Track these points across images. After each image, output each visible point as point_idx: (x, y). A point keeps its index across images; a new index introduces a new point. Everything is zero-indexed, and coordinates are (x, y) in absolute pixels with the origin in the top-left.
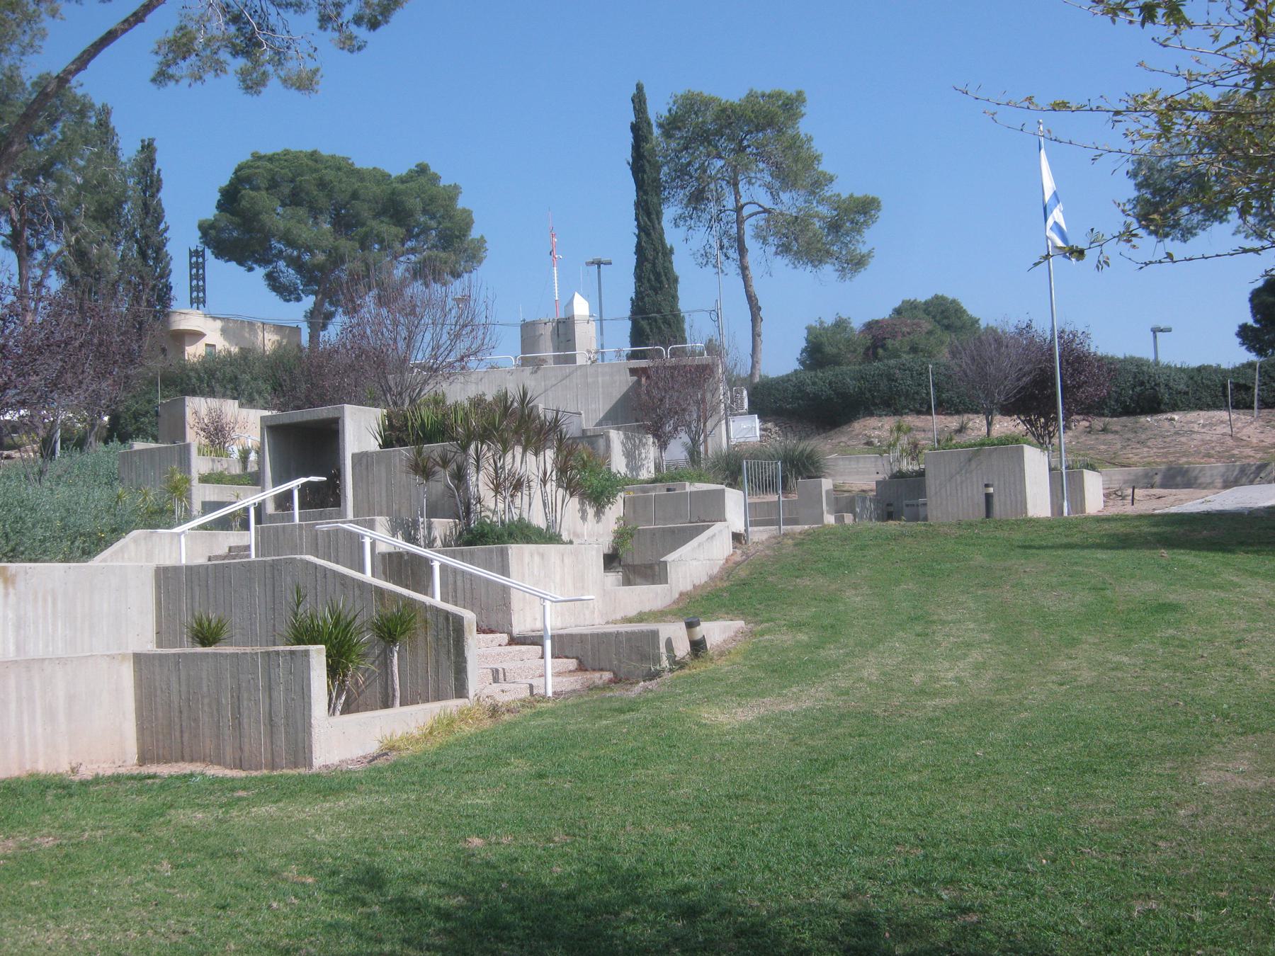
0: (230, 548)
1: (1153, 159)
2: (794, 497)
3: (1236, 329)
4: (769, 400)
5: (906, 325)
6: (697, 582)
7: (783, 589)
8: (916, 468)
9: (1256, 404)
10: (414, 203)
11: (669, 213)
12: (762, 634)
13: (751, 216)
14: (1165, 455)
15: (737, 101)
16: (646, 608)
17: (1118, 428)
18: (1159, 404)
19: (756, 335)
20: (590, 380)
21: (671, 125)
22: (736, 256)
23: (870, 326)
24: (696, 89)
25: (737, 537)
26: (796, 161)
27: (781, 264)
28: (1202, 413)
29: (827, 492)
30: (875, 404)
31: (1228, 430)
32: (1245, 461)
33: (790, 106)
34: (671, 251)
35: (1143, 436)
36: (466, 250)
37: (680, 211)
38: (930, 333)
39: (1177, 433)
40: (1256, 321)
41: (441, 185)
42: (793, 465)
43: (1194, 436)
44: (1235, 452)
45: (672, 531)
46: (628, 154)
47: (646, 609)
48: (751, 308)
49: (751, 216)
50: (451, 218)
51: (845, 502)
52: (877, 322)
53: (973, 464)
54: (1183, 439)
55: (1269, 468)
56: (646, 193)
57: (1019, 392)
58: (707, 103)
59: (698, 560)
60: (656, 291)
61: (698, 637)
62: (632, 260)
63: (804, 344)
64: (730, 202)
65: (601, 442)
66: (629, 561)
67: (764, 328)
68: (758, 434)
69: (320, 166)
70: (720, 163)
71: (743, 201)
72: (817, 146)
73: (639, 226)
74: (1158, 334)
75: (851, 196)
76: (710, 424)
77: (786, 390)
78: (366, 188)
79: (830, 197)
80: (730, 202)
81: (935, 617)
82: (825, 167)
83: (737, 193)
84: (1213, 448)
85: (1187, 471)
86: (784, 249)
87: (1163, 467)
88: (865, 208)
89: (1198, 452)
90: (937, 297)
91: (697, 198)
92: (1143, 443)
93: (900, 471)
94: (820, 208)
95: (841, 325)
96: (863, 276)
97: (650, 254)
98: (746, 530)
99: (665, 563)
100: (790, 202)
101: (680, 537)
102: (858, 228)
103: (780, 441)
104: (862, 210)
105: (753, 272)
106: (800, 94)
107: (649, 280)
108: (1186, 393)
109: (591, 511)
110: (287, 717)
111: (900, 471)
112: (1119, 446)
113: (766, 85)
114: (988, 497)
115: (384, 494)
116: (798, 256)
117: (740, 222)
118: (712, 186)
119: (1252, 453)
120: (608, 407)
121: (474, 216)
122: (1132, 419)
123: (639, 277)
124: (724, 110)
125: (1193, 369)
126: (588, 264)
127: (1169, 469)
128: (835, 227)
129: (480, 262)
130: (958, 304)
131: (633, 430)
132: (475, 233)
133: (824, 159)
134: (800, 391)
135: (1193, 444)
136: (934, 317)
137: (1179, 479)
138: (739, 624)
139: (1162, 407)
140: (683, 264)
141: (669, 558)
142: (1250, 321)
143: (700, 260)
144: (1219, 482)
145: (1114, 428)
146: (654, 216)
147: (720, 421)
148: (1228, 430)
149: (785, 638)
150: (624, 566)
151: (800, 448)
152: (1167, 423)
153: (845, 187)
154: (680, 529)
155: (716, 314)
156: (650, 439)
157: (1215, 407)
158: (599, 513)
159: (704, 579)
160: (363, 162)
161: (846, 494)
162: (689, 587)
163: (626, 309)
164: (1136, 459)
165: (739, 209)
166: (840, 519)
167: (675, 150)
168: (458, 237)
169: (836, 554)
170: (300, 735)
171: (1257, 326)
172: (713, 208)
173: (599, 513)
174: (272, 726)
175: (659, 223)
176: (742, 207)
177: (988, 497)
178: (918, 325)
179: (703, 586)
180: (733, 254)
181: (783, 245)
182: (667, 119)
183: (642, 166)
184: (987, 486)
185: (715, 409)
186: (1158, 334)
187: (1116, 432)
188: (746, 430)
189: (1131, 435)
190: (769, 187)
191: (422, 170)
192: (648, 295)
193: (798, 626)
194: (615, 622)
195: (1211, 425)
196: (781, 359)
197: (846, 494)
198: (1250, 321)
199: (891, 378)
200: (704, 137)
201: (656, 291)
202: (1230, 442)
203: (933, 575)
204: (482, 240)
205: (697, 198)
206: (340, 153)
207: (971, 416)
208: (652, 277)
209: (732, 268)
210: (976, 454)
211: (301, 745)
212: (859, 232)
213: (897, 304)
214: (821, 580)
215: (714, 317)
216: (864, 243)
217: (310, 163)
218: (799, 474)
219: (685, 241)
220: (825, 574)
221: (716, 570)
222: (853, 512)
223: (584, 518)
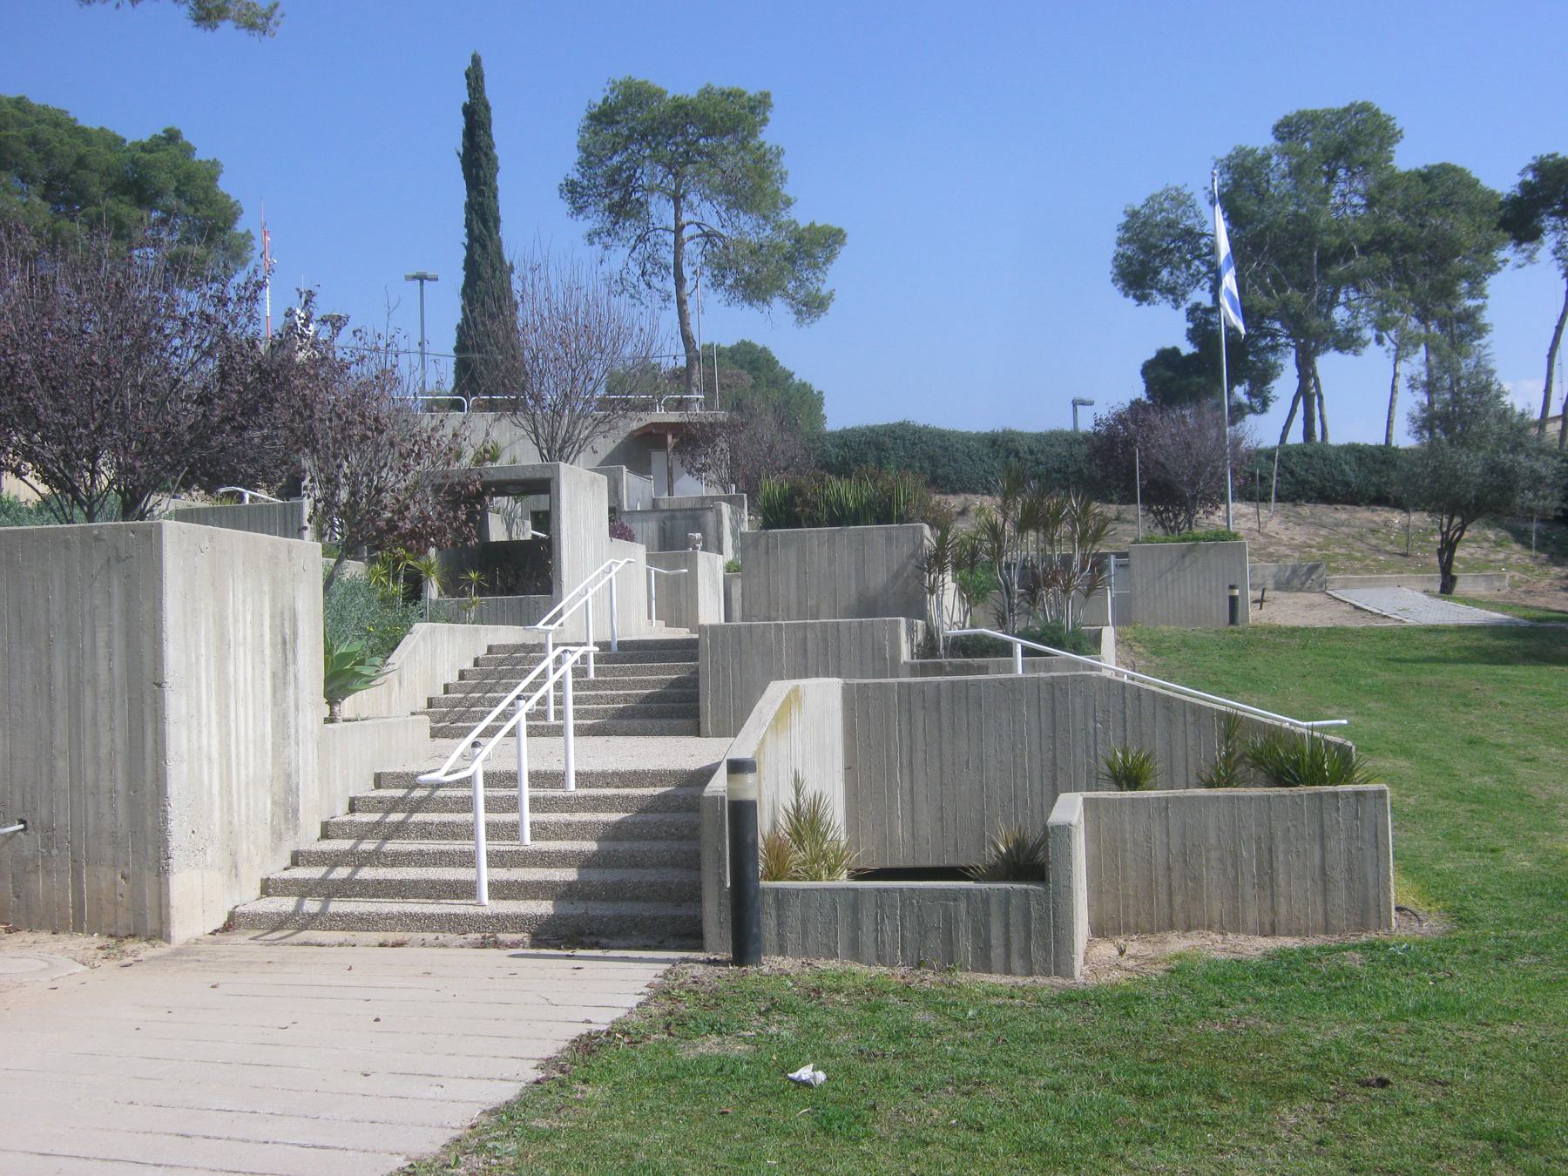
0: (490, 649)
10: (162, 178)
13: (692, 238)
40: (1149, 397)
41: (196, 159)
46: (457, 142)
53: (1187, 562)
62: (460, 278)
69: (31, 119)
73: (470, 235)
78: (98, 153)
90: (743, 343)
96: (824, 321)
100: (747, 228)
104: (819, 244)
110: (1350, 870)
113: (723, 81)
114: (1233, 599)
115: (793, 585)
119: (1288, 552)
130: (769, 353)
132: (240, 227)
153: (804, 213)
160: (89, 119)
163: (451, 340)
170: (1372, 893)
174: (1325, 882)
177: (1233, 599)
183: (477, 159)
184: (1232, 587)
191: (172, 137)
206: (56, 103)
210: (1190, 549)
211: (1372, 902)
217: (17, 113)
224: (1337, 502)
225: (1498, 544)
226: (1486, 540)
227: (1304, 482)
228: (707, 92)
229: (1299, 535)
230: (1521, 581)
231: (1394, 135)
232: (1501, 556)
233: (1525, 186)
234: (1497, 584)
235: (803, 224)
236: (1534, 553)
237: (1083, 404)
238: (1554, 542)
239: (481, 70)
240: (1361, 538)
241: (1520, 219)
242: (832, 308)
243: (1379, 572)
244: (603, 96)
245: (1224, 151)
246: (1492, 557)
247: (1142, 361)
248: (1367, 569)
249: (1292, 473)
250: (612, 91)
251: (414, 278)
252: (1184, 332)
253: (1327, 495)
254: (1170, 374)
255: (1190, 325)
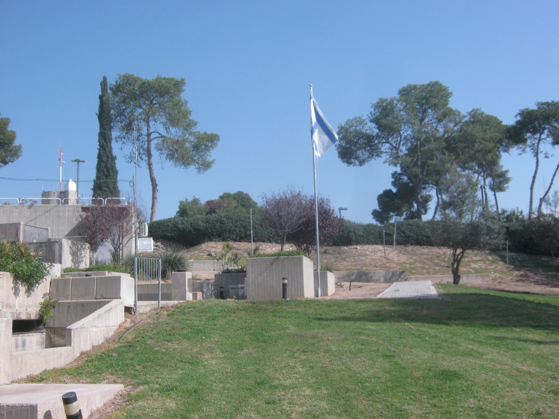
1: (347, 126)
2: (169, 282)
3: (372, 211)
4: (158, 231)
5: (226, 203)
6: (96, 344)
7: (158, 351)
8: (236, 268)
9: (394, 242)
11: (115, 134)
12: (137, 398)
13: (155, 138)
14: (356, 265)
15: (151, 80)
16: (51, 366)
17: (331, 252)
18: (350, 241)
19: (154, 198)
20: (61, 214)
21: (117, 89)
22: (146, 158)
23: (209, 203)
24: (130, 73)
25: (128, 310)
26: (179, 112)
27: (169, 164)
28: (370, 246)
29: (189, 280)
30: (213, 235)
31: (383, 255)
32: (394, 270)
33: (178, 85)
34: (115, 158)
35: (344, 256)
36: (11, 151)
37: (118, 134)
38: (236, 207)
39: (359, 255)
40: (380, 208)
42: (170, 264)
43: (368, 257)
44: (388, 265)
45: (83, 304)
46: (96, 109)
47: (50, 367)
48: (152, 185)
49: (155, 138)
50: (4, 134)
51: (198, 286)
52: (212, 201)
53: (274, 266)
54: (363, 258)
55: (405, 273)
56: (105, 129)
57: (299, 227)
58: (136, 80)
59: (95, 329)
60: (107, 177)
61: (74, 412)
62: (96, 161)
63: (178, 209)
64: (144, 131)
65: (57, 246)
66: (51, 325)
67: (158, 195)
68: (152, 247)
70: (140, 111)
71: (151, 131)
72: (190, 106)
73: (100, 145)
74: (342, 211)
75: (205, 133)
76: (125, 240)
77: (168, 226)
79: (195, 133)
80: (144, 131)
81: (276, 382)
82: (192, 117)
83: (148, 126)
84: (377, 263)
85: (367, 274)
86: (171, 156)
87: (356, 271)
88: (212, 139)
89: (370, 265)
90: (239, 192)
91: (128, 128)
92: (344, 259)
93: (228, 269)
94: (190, 137)
95: (196, 201)
96: (209, 172)
97: (104, 159)
98: (135, 305)
99: (70, 330)
100: (175, 133)
101: (86, 309)
102: (207, 148)
103: (163, 251)
105: (155, 167)
106: (183, 80)
107: (103, 171)
108: (363, 236)
109: (22, 289)
111: (228, 269)
112: (333, 260)
114: (284, 285)
116: (177, 160)
117: (149, 141)
118: (136, 122)
119: (395, 266)
120: (70, 229)
121: (17, 135)
122: (337, 248)
123: (98, 170)
124: (144, 83)
125: (365, 226)
126: (73, 161)
127: (359, 273)
128: (196, 147)
129: (18, 157)
131: (77, 240)
132: (16, 143)
133: (193, 113)
134: (175, 227)
135: (368, 260)
136: (238, 201)
137: (363, 277)
138: (119, 387)
139: (352, 242)
140: (121, 165)
141: (73, 326)
142: (377, 208)
143: (128, 160)
144: (382, 279)
145: (330, 252)
146: (108, 141)
147: (131, 238)
148: (383, 255)
149: (156, 404)
150: (47, 328)
151: (174, 255)
152: (354, 250)
153: (204, 127)
154: (88, 303)
155: (133, 184)
156: (88, 245)
157: (376, 243)
158: (29, 290)
159: (101, 340)
161: (198, 281)
162: (89, 348)
164: (341, 267)
165: (149, 135)
166: (195, 296)
167: (117, 102)
168: (7, 144)
169: (196, 323)
171: (380, 210)
172: (135, 133)
173: (29, 290)
175: (110, 144)
176: (151, 134)
178: (231, 203)
179: (100, 347)
180: (145, 158)
181: (170, 154)
182: (115, 86)
184: (284, 279)
185: (128, 232)
186: (342, 211)
187: (331, 254)
188: (146, 245)
189: (338, 255)
190: (164, 124)
192: (103, 179)
193: (166, 390)
194: (18, 382)
195: (375, 252)
196: (167, 211)
197: (198, 281)
198: (377, 208)
199: (222, 222)
200: (133, 96)
201: (107, 177)
202: (385, 260)
203: (264, 341)
204: (20, 147)
205: (128, 128)
207: (261, 243)
208: (105, 170)
209: (144, 165)
210: (275, 260)
212: (209, 151)
213: (221, 194)
214: (186, 344)
215: (132, 184)
216: (210, 156)
218: (173, 269)
219: (121, 150)
220: (188, 339)
221: (111, 334)
222: (202, 291)
223: (16, 293)
224: (425, 245)
225: (493, 262)
226: (488, 260)
227: (408, 237)
228: (158, 79)
229: (403, 258)
230: (499, 278)
231: (448, 95)
232: (493, 267)
233: (518, 123)
234: (486, 279)
235: (202, 132)
236: (507, 265)
237: (343, 209)
238: (519, 261)
239: (106, 82)
240: (431, 260)
241: (515, 136)
242: (214, 167)
243: (433, 274)
244: (115, 80)
245: (375, 101)
246: (489, 267)
247: (377, 195)
248: (429, 273)
249: (404, 233)
250: (119, 78)
251: (75, 161)
252: (391, 183)
253: (419, 242)
254: (387, 199)
255: (393, 180)
